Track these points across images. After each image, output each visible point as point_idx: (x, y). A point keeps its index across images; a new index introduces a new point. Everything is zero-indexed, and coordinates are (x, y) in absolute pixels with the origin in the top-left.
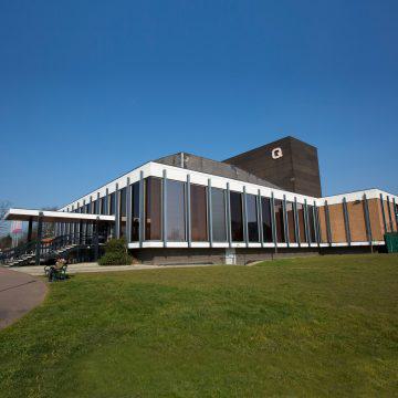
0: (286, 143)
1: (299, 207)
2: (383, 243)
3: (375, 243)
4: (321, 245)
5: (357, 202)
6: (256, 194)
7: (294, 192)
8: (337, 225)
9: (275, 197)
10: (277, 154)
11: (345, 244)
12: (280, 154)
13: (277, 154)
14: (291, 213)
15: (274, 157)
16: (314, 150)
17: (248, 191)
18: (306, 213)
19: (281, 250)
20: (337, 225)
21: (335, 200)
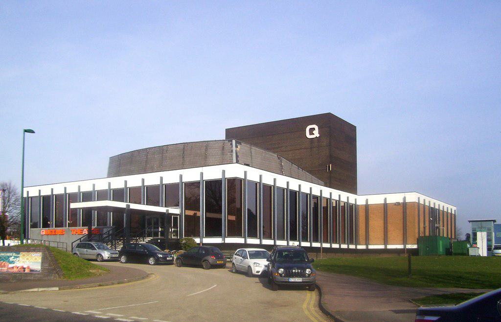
0: (328, 122)
1: (342, 204)
2: (415, 247)
3: (409, 246)
4: (359, 247)
5: (398, 204)
6: (308, 192)
7: (330, 187)
8: (376, 224)
9: (249, 178)
10: (313, 132)
11: (382, 247)
12: (316, 134)
13: (313, 132)
14: (326, 209)
15: (308, 136)
16: (353, 128)
17: (278, 184)
18: (445, 214)
19: (325, 250)
20: (376, 224)
21: (376, 200)
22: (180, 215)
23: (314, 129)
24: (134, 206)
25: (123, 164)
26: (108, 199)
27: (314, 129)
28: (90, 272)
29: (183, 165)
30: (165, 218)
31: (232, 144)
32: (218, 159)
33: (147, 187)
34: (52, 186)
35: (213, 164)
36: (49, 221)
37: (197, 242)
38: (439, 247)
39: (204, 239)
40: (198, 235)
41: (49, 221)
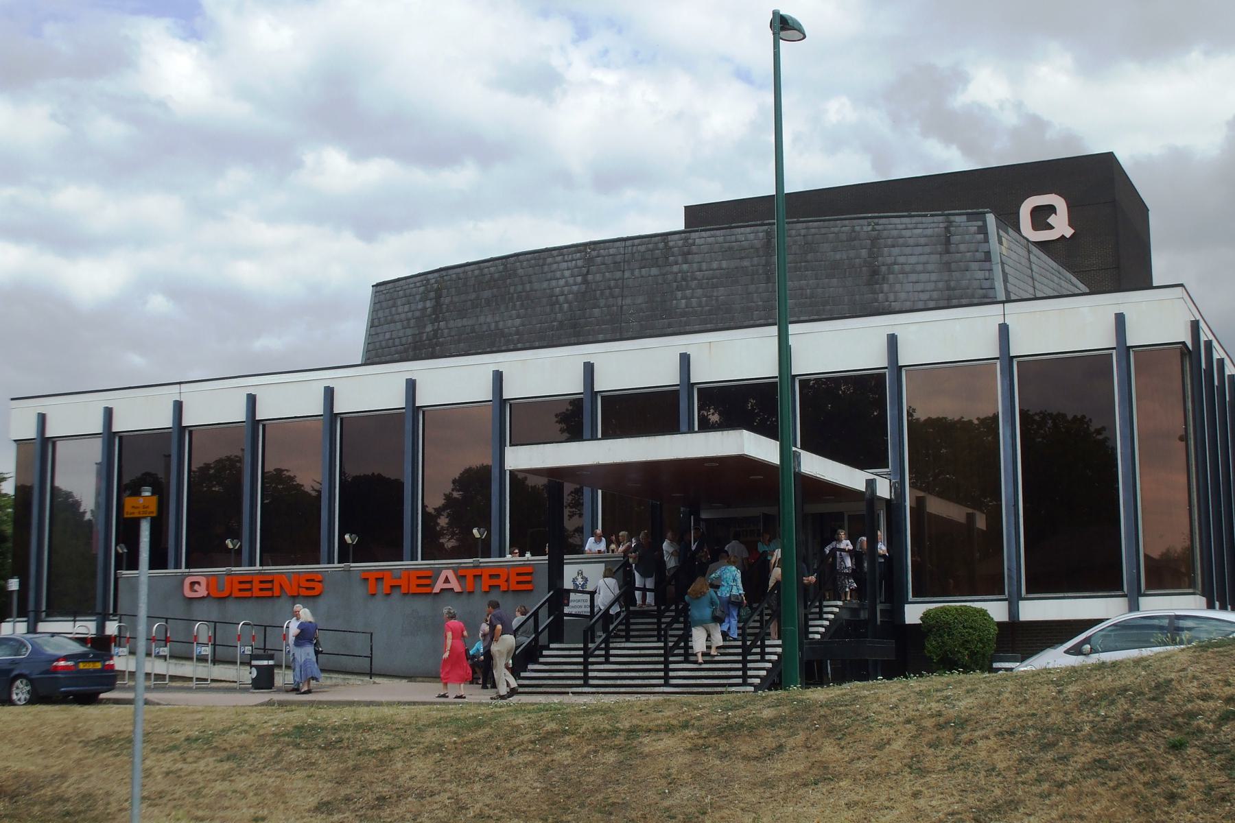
22: (893, 507)
23: (1051, 209)
24: (814, 465)
25: (423, 314)
26: (683, 426)
27: (1051, 209)
28: (56, 667)
29: (658, 320)
30: (826, 508)
31: (983, 230)
32: (931, 286)
33: (805, 383)
34: (327, 378)
35: (908, 305)
36: (236, 535)
37: (996, 619)
38: (167, 536)
39: (1021, 603)
40: (993, 587)
41: (236, 535)
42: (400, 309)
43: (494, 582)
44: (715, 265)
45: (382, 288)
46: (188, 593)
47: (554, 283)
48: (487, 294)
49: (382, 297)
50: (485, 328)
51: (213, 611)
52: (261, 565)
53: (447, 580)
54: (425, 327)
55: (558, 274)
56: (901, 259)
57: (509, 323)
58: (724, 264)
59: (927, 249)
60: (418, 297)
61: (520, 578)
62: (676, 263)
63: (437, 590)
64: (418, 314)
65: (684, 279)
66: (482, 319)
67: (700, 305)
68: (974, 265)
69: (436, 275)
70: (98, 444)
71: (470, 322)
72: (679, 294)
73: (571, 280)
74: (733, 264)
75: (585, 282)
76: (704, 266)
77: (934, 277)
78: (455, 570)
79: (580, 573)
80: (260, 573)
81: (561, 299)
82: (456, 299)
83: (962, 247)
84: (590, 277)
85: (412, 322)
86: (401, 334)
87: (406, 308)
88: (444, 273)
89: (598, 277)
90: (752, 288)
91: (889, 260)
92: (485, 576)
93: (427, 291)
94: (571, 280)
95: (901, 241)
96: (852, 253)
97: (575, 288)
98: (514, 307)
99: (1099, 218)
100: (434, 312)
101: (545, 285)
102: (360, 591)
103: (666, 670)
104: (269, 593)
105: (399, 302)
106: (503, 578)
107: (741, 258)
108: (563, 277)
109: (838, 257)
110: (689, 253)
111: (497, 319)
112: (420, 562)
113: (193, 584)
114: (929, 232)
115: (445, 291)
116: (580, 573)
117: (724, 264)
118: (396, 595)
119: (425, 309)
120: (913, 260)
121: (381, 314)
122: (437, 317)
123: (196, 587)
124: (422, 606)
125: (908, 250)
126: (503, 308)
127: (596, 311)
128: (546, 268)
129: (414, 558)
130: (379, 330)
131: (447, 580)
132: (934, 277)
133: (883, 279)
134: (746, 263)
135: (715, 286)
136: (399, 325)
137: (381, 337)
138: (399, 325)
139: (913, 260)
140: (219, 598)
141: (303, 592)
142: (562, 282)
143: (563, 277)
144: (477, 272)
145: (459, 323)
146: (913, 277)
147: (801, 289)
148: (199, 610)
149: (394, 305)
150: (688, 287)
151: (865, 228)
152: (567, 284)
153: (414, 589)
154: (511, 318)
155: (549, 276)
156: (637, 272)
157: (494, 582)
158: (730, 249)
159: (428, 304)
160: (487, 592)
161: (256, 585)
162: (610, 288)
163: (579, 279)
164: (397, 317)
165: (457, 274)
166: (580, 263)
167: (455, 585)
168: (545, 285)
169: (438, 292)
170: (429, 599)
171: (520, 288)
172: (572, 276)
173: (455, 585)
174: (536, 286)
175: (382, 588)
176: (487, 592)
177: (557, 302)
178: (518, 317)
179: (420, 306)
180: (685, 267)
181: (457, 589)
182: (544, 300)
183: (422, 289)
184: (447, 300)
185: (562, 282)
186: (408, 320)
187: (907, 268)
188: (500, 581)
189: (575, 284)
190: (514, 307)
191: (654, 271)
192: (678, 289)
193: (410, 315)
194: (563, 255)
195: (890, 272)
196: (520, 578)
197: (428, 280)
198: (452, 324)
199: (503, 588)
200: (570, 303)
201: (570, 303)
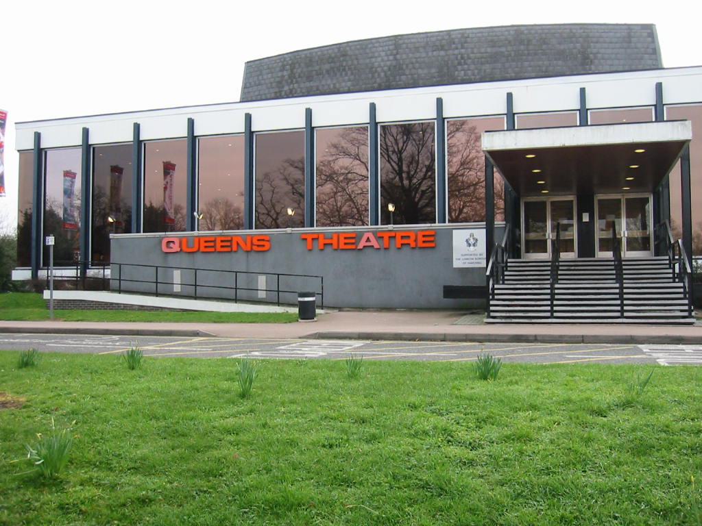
42: (265, 77)
43: (405, 241)
44: (483, 50)
45: (252, 64)
46: (165, 249)
47: (373, 60)
48: (327, 66)
49: (252, 70)
50: (326, 87)
51: (185, 260)
52: (317, 226)
53: (368, 240)
54: (283, 87)
55: (376, 54)
56: (602, 51)
57: (343, 84)
58: (489, 50)
59: (618, 45)
60: (278, 69)
61: (425, 239)
62: (457, 48)
63: (360, 247)
64: (277, 79)
65: (462, 58)
66: (323, 82)
67: (473, 75)
68: (646, 56)
69: (290, 55)
70: (80, 151)
71: (315, 84)
72: (459, 67)
73: (386, 58)
74: (494, 50)
75: (395, 59)
76: (475, 51)
77: (622, 62)
78: (374, 233)
79: (472, 235)
80: (221, 235)
81: (379, 69)
82: (305, 70)
83: (639, 45)
84: (398, 57)
85: (274, 85)
86: (267, 92)
87: (270, 76)
88: (296, 54)
89: (404, 56)
90: (507, 65)
91: (595, 51)
92: (398, 237)
93: (283, 66)
94: (386, 58)
95: (601, 40)
96: (571, 46)
97: (388, 63)
98: (346, 75)
99: (634, 48)
100: (290, 77)
101: (368, 61)
102: (300, 247)
103: (622, 305)
104: (229, 249)
105: (264, 72)
106: (413, 238)
107: (500, 47)
108: (379, 56)
109: (562, 47)
110: (466, 42)
111: (334, 82)
112: (379, 226)
113: (169, 242)
114: (618, 35)
115: (297, 66)
116: (472, 235)
117: (489, 50)
118: (328, 250)
119: (283, 76)
120: (609, 51)
121: (251, 80)
122: (292, 81)
123: (172, 245)
124: (348, 257)
125: (606, 45)
126: (338, 74)
127: (403, 78)
128: (368, 51)
129: (138, 231)
130: (250, 90)
131: (368, 240)
132: (622, 62)
133: (591, 62)
134: (503, 49)
135: (482, 64)
136: (264, 87)
137: (252, 94)
138: (264, 87)
139: (609, 51)
140: (189, 253)
141: (255, 248)
142: (379, 59)
143: (379, 56)
144: (319, 53)
145: (308, 84)
146: (609, 62)
147: (539, 66)
148: (172, 261)
149: (261, 74)
150: (465, 64)
151: (579, 31)
152: (383, 60)
153: (342, 246)
154: (344, 81)
155: (370, 55)
156: (430, 54)
157: (405, 241)
158: (492, 41)
159: (285, 73)
160: (322, 250)
161: (219, 244)
162: (412, 63)
163: (391, 58)
164: (263, 82)
165: (306, 55)
166: (391, 47)
167: (374, 242)
168: (368, 61)
169: (293, 66)
170: (354, 253)
171: (350, 63)
172: (387, 55)
173: (374, 242)
174: (361, 61)
175: (317, 245)
176: (322, 250)
177: (376, 71)
178: (349, 80)
179: (280, 74)
180: (463, 51)
181: (376, 246)
182: (367, 70)
183: (280, 64)
184: (299, 71)
185: (379, 59)
186: (271, 83)
187: (606, 56)
188: (411, 241)
189: (388, 60)
190: (346, 75)
191: (442, 53)
192: (459, 64)
193: (272, 80)
194: (379, 42)
195: (596, 58)
196: (425, 239)
197: (285, 59)
198: (302, 85)
199: (413, 245)
200: (385, 72)
201: (385, 72)
